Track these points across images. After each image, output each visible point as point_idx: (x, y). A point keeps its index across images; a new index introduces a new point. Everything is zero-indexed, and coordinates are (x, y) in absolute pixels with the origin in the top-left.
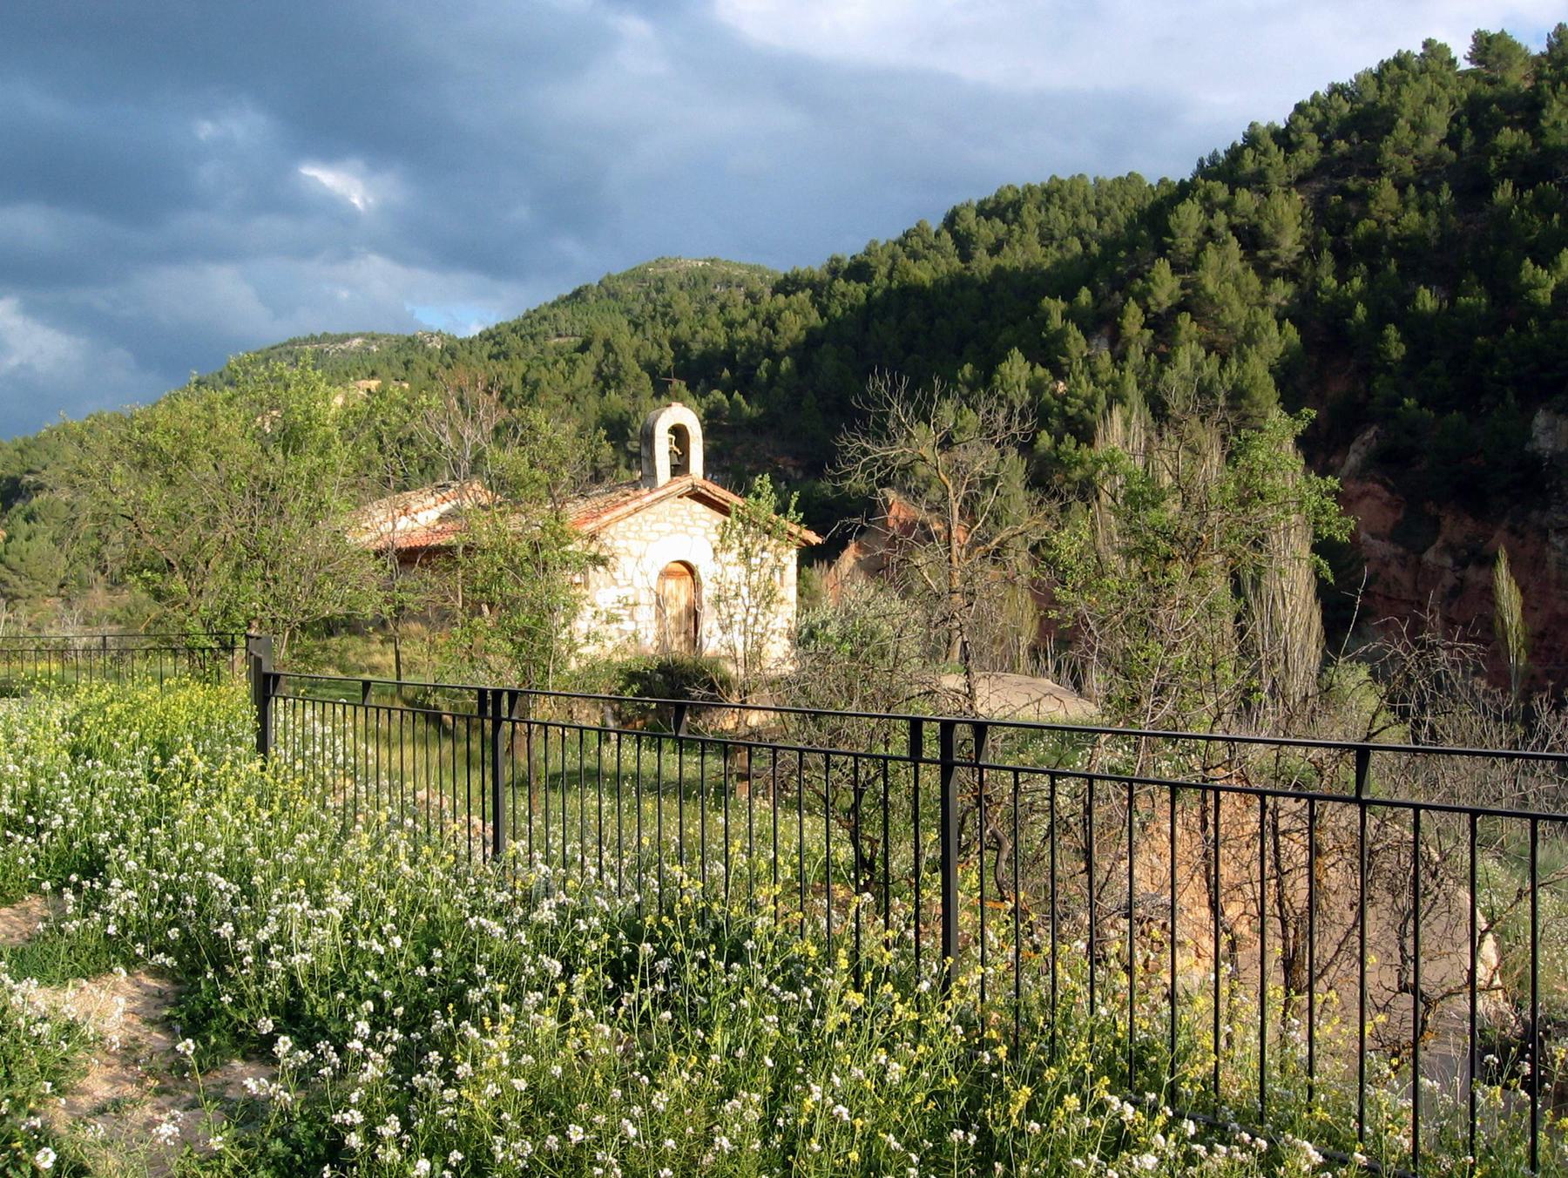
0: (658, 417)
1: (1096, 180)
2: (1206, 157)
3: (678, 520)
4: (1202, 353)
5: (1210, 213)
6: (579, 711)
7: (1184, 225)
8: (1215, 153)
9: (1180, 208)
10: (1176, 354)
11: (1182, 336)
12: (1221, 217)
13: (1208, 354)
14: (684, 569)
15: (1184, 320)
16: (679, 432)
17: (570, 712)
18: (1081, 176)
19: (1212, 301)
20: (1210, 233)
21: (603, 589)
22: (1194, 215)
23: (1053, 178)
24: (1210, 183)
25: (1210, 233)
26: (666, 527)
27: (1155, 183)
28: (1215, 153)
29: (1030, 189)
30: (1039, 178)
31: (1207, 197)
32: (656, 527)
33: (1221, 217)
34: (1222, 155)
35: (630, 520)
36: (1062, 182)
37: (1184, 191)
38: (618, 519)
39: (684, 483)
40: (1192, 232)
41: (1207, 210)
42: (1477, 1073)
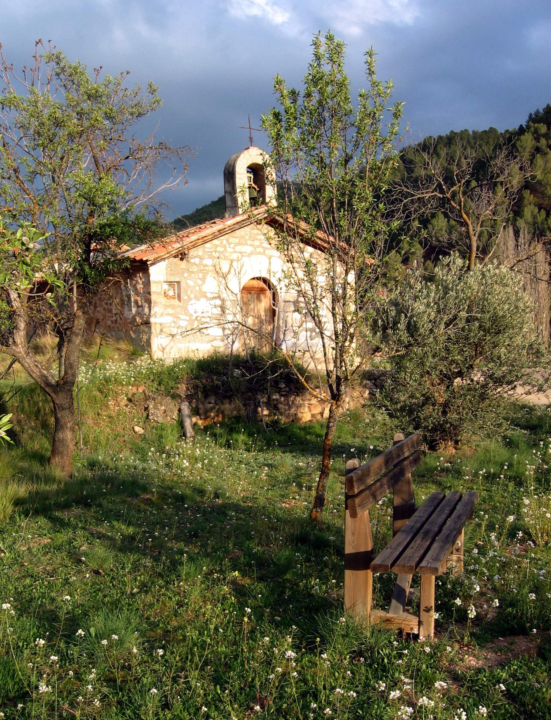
0: (238, 157)
1: (473, 131)
2: (533, 113)
3: (257, 243)
4: (536, 210)
5: (537, 139)
6: (155, 408)
7: (524, 146)
8: (538, 111)
9: (522, 137)
10: (523, 211)
11: (526, 202)
12: (543, 141)
13: (540, 210)
14: (262, 284)
15: (527, 194)
16: (256, 170)
17: (146, 409)
18: (466, 130)
19: (541, 184)
20: (538, 150)
21: (194, 301)
22: (529, 141)
23: (452, 132)
24: (536, 125)
25: (538, 150)
26: (248, 249)
27: (503, 132)
28: (538, 111)
29: (440, 137)
30: (445, 132)
31: (536, 131)
32: (238, 248)
33: (543, 141)
34: (541, 111)
35: (216, 242)
36: (456, 134)
37: (522, 131)
38: (205, 241)
39: (260, 211)
40: (528, 150)
41: (535, 139)
42: (402, 458)
